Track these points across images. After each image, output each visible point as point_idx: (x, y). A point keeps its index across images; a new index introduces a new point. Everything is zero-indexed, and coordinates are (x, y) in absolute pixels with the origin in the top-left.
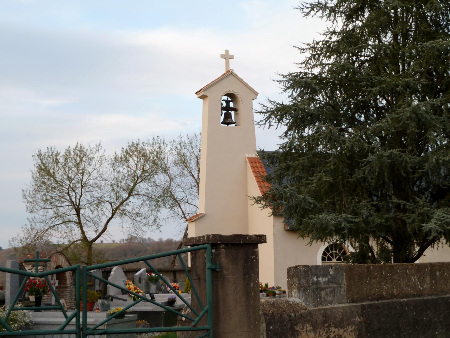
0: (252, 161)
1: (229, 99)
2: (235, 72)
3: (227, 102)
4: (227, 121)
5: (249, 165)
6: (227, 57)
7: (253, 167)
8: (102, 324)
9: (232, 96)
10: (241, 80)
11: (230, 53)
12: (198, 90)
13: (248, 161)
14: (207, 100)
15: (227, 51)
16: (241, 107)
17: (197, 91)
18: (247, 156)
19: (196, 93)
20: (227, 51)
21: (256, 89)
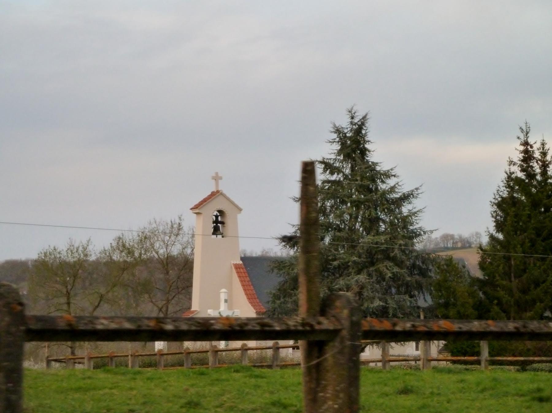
0: (237, 267)
1: (218, 214)
2: (225, 192)
3: (217, 217)
4: (216, 231)
5: (234, 271)
6: (217, 178)
7: (238, 272)
8: (149, 318)
9: (221, 212)
10: (228, 199)
11: (220, 175)
12: (201, 199)
13: (233, 268)
14: (201, 217)
15: (217, 173)
16: (229, 221)
17: (197, 202)
18: (232, 263)
19: (191, 209)
20: (217, 173)
21: (241, 206)
